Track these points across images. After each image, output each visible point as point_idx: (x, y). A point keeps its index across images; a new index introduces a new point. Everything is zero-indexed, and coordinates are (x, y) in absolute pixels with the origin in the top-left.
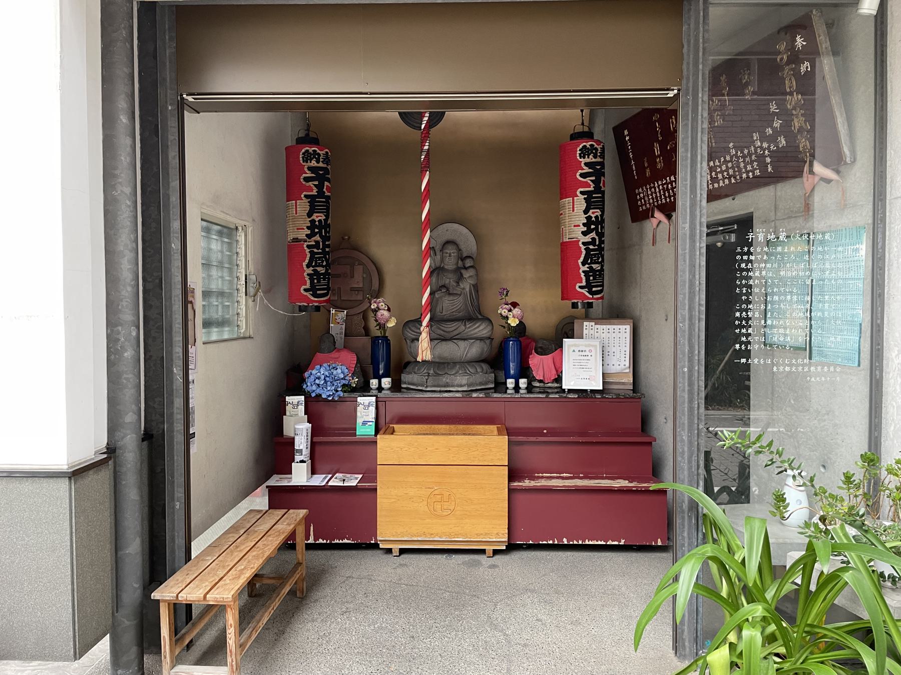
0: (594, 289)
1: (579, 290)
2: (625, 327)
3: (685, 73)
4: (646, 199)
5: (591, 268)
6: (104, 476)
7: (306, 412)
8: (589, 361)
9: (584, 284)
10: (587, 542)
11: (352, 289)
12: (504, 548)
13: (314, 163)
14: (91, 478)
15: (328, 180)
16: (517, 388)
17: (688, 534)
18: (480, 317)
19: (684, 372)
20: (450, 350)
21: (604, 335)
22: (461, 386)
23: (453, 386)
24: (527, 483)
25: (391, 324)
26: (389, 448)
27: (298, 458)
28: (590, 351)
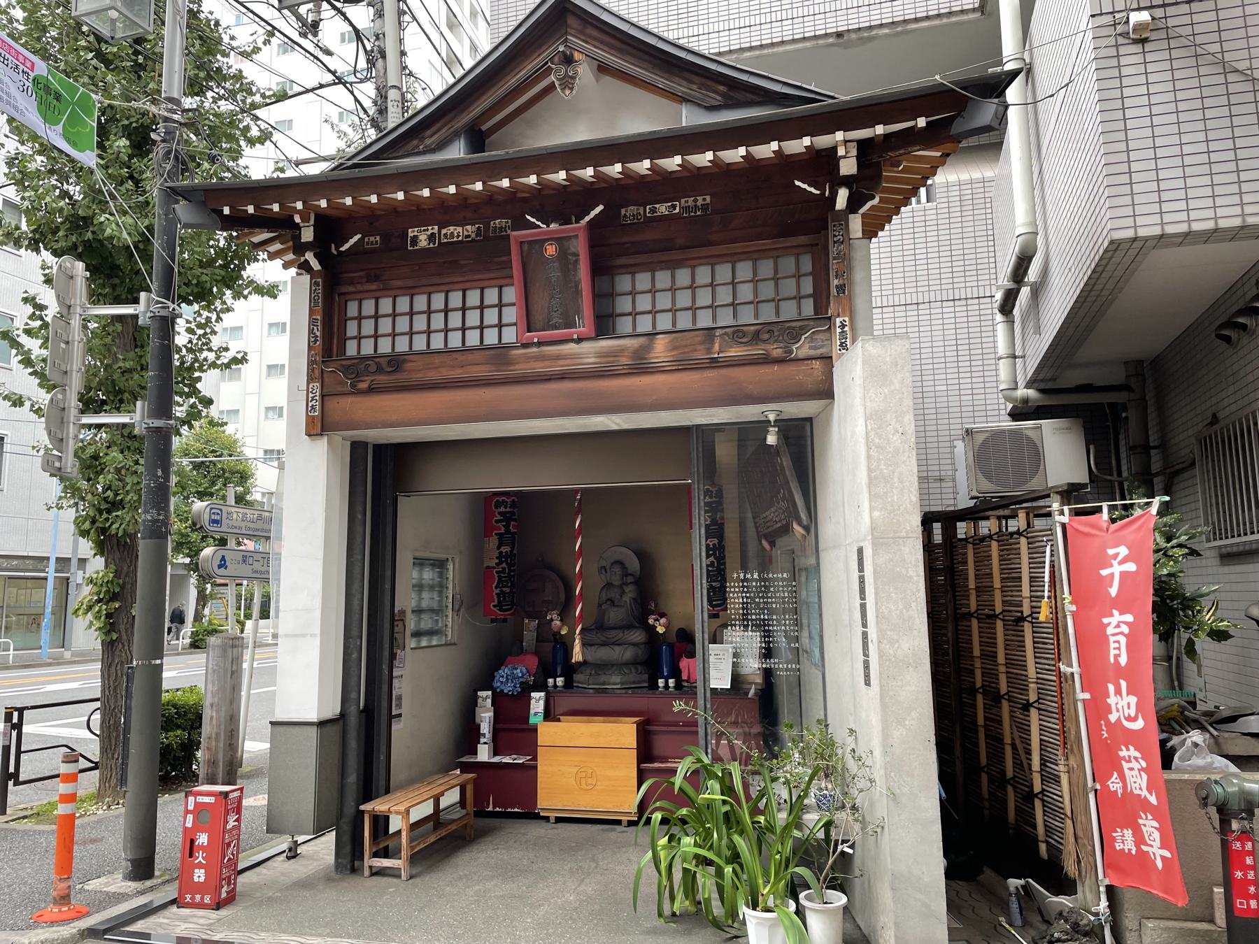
6: (337, 728)
7: (493, 705)
11: (544, 602)
13: (502, 509)
14: (329, 728)
15: (515, 520)
16: (667, 687)
20: (604, 654)
26: (547, 733)
27: (482, 740)
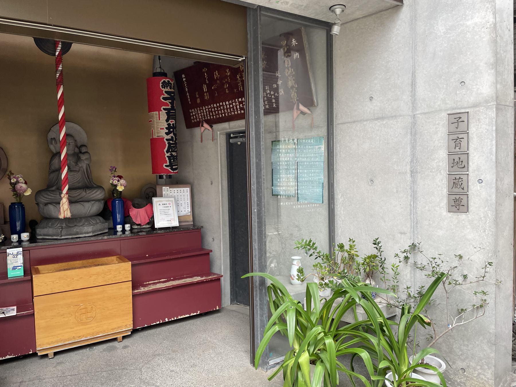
0: (174, 167)
1: (165, 167)
2: (186, 189)
3: (249, 49)
4: (197, 115)
5: (171, 154)
8: (168, 210)
9: (168, 164)
10: (179, 318)
12: (130, 333)
16: (124, 230)
17: (260, 299)
18: (95, 186)
19: (255, 212)
21: (175, 194)
22: (88, 233)
23: (81, 234)
24: (142, 290)
25: (28, 193)
28: (169, 204)
